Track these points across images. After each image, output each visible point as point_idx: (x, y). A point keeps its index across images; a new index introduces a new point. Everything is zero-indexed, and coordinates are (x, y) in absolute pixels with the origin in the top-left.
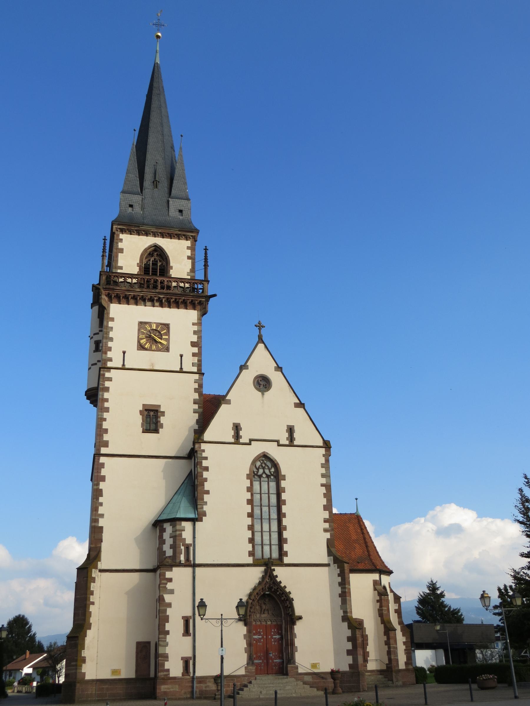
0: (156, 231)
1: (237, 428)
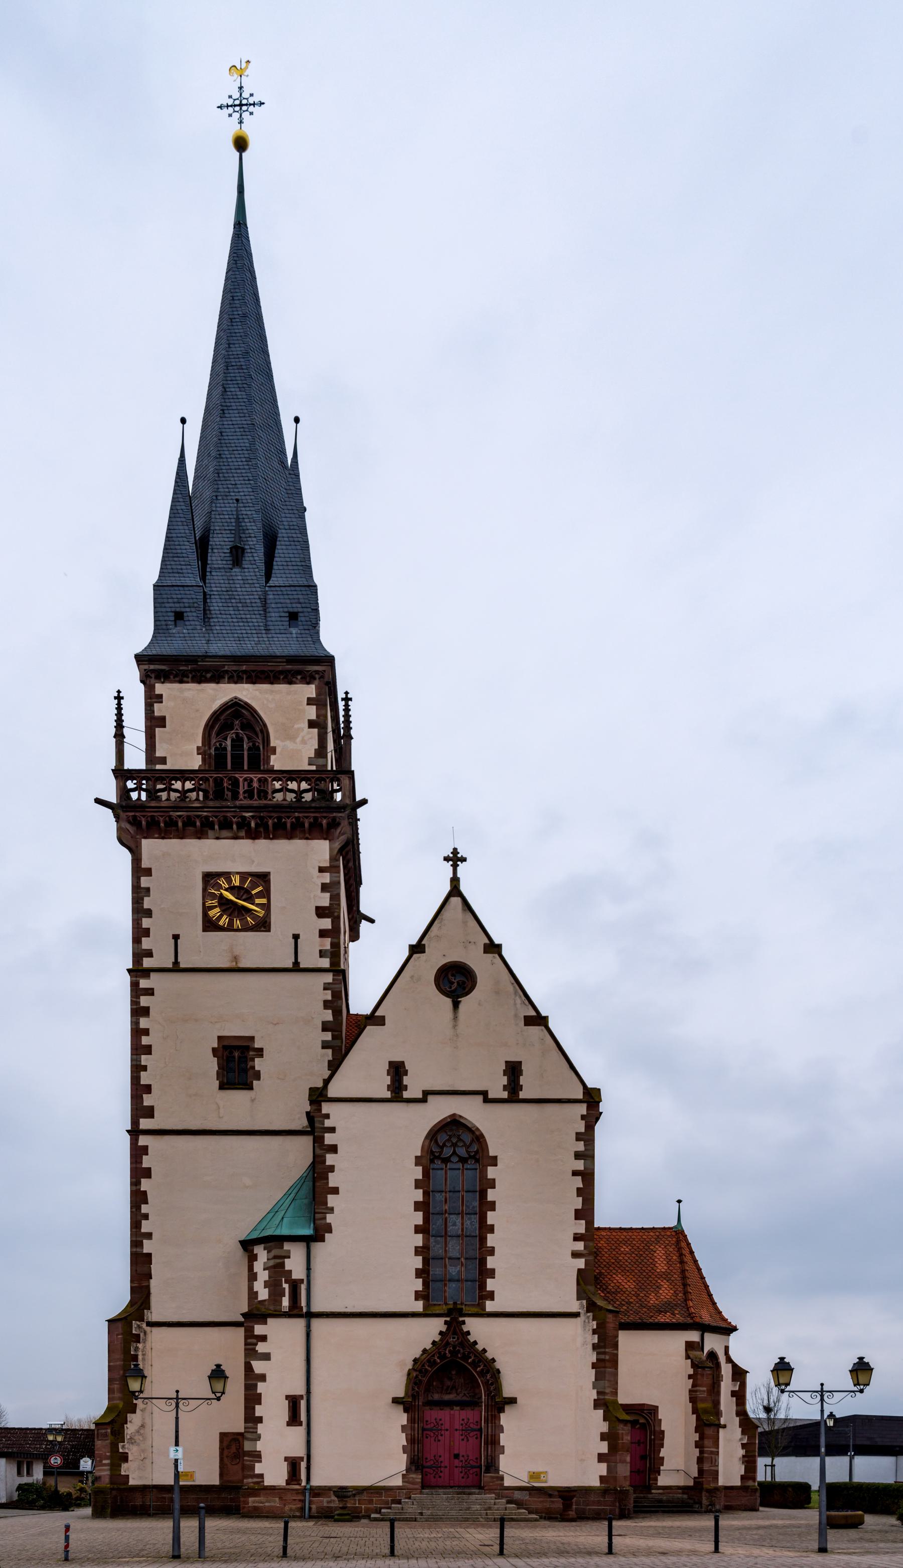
0: (235, 668)
1: (397, 1070)
